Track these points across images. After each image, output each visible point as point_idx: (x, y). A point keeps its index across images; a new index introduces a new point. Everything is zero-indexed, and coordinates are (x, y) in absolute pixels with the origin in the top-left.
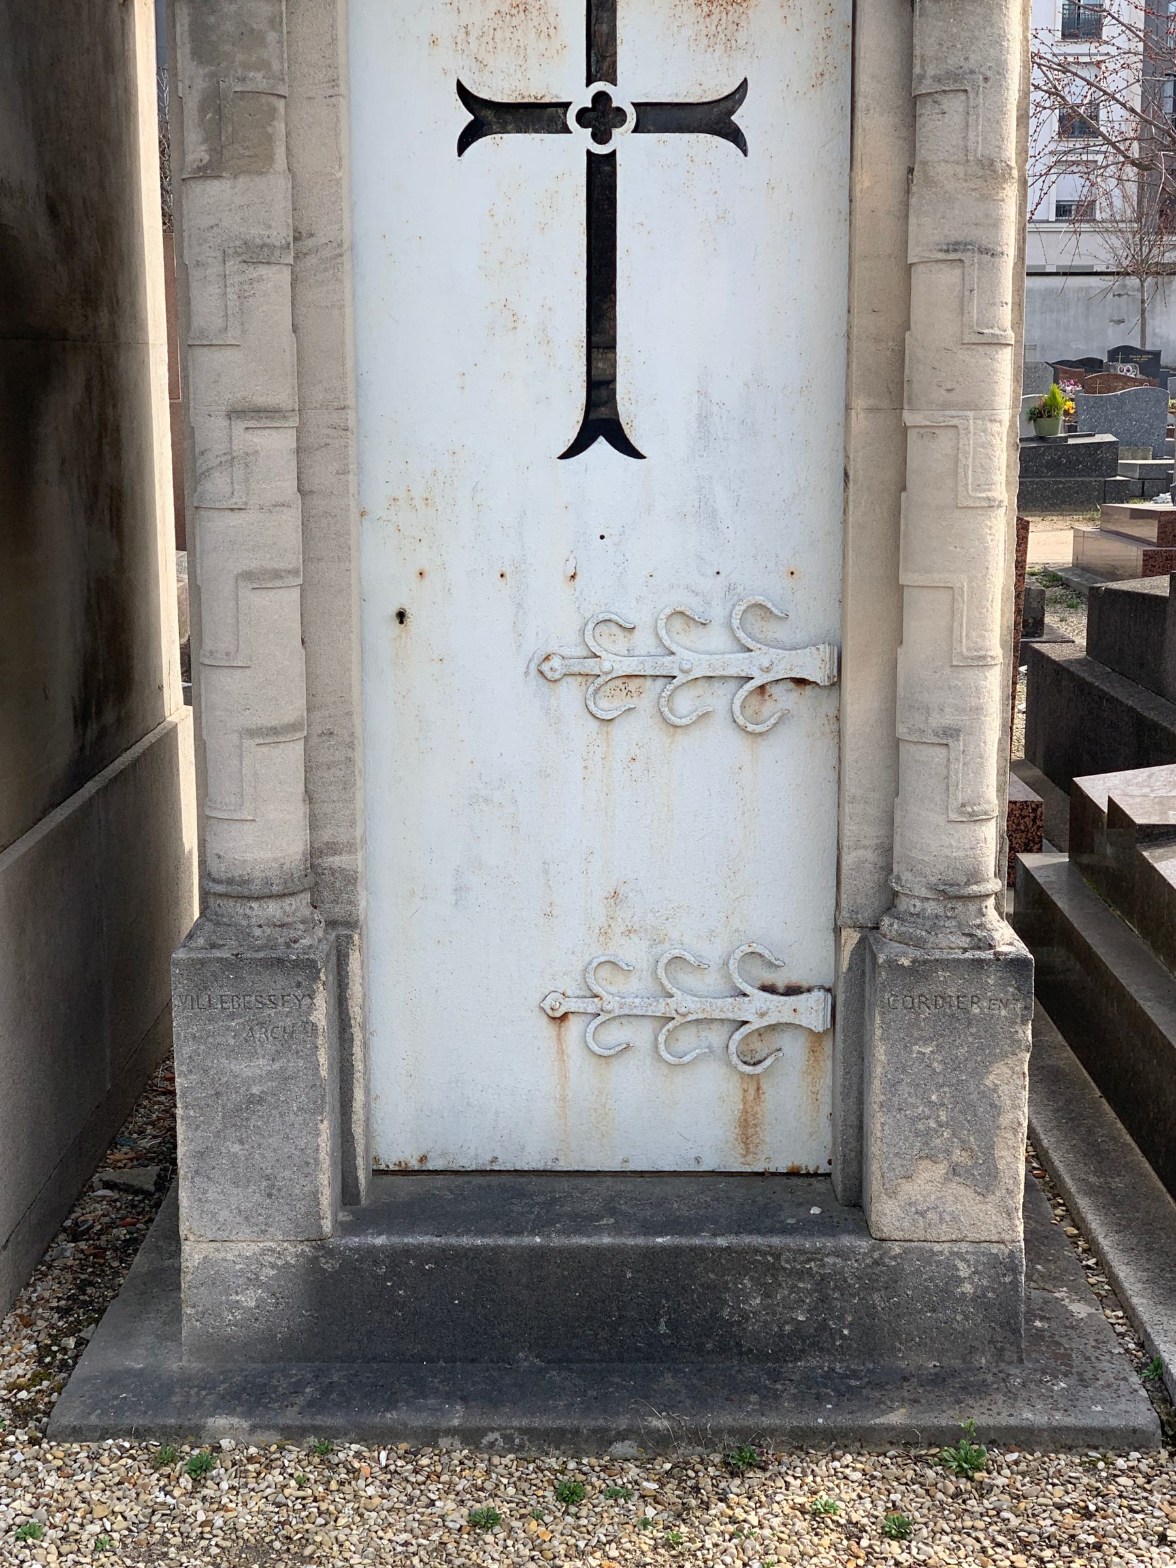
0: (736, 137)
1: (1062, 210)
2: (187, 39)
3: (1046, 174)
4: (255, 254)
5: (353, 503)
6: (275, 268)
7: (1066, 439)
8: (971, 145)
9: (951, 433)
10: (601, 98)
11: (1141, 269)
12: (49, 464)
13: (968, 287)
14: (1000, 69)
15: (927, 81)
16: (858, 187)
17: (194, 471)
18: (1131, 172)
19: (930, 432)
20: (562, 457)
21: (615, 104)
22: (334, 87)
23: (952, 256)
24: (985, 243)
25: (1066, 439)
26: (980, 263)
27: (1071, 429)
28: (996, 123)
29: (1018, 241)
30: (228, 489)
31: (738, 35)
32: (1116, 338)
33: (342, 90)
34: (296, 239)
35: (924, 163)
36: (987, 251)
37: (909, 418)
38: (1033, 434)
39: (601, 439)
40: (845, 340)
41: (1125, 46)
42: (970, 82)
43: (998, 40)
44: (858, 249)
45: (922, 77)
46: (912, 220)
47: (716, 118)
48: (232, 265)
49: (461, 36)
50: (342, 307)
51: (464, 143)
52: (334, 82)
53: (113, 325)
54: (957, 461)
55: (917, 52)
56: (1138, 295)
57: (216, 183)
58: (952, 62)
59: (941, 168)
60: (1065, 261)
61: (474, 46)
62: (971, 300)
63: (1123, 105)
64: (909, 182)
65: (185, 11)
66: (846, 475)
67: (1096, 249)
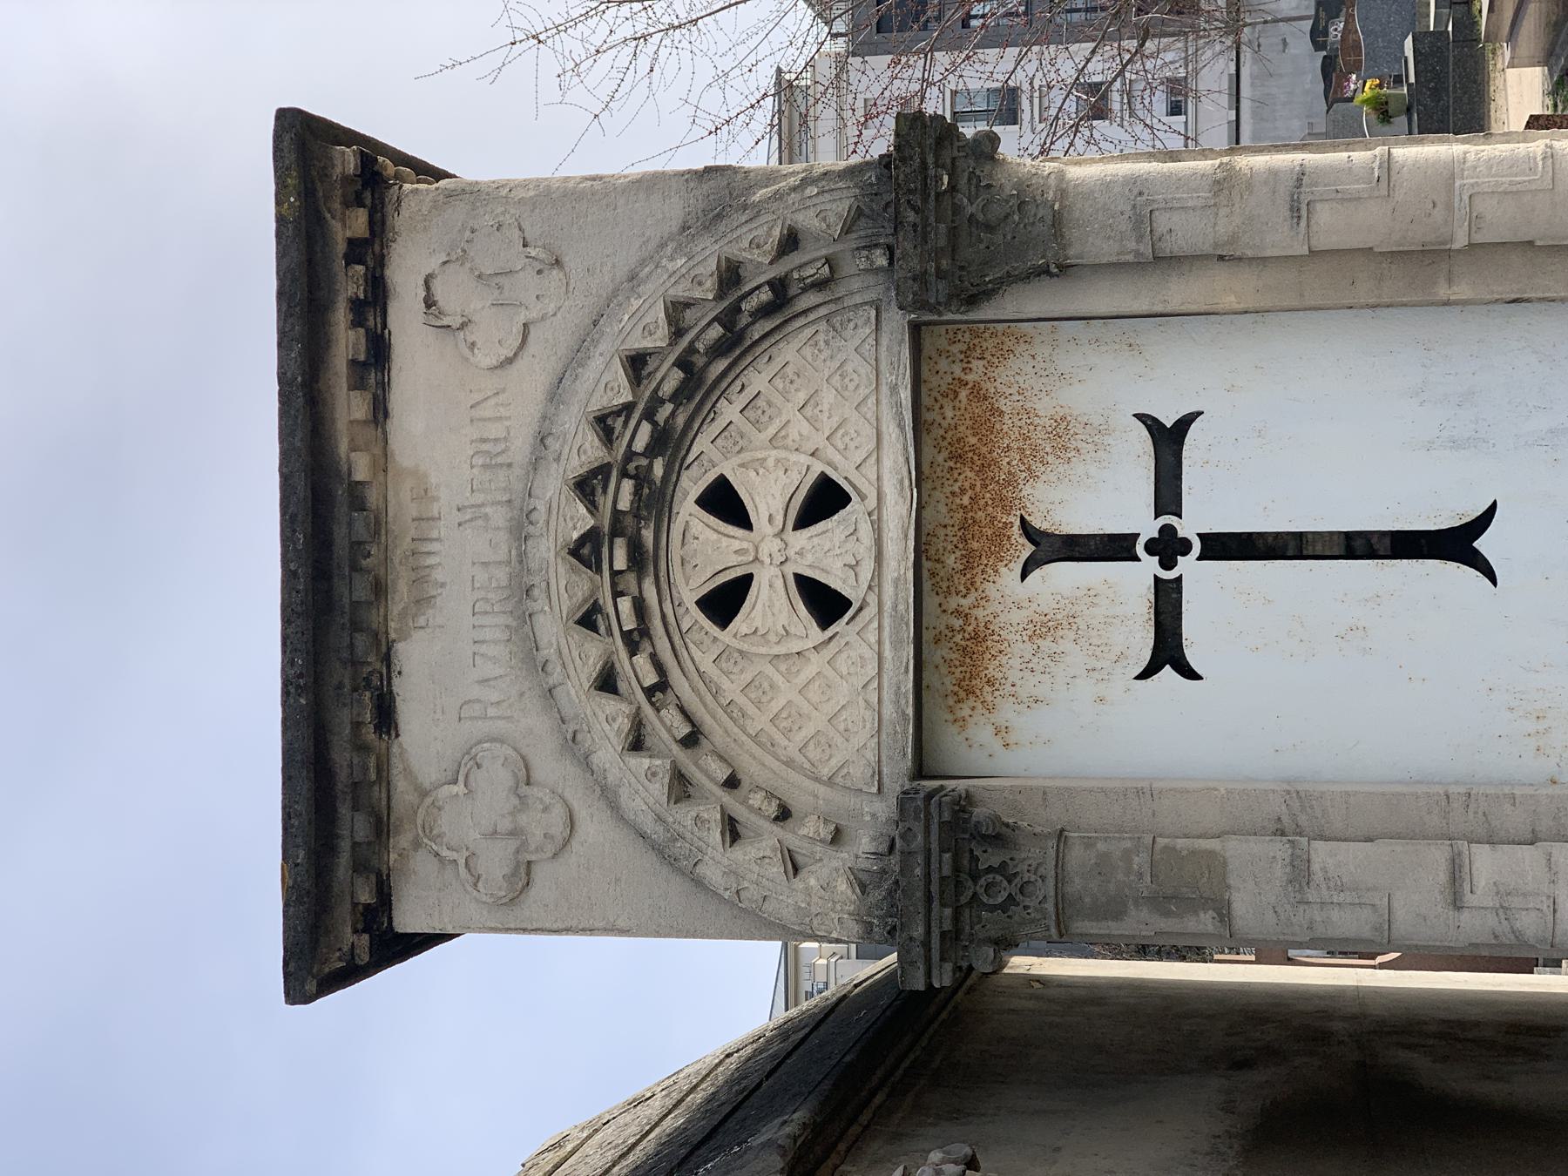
0: (1185, 423)
1: (1175, 109)
2: (1104, 924)
3: (1151, 128)
4: (1300, 873)
5: (1544, 791)
6: (1313, 856)
7: (1409, 85)
8: (1201, 202)
9: (1477, 201)
10: (1151, 548)
11: (1233, 27)
12: (1492, 1090)
13: (1334, 195)
14: (1132, 181)
15: (1142, 248)
16: (1236, 307)
17: (1511, 946)
18: (1150, 45)
19: (1475, 221)
20: (1494, 583)
21: (1156, 535)
22: (1144, 792)
23: (1304, 213)
24: (1291, 183)
25: (1409, 85)
26: (1311, 185)
27: (1398, 80)
28: (1180, 181)
29: (1287, 152)
30: (1533, 914)
31: (1096, 424)
32: (1301, 45)
33: (1145, 784)
34: (1283, 834)
35: (1216, 245)
36: (1300, 180)
37: (1460, 242)
38: (1404, 119)
39: (1475, 544)
40: (1378, 310)
41: (1035, 63)
42: (1142, 206)
43: (1107, 185)
44: (1295, 304)
45: (1137, 253)
46: (1268, 253)
47: (1168, 440)
48: (1311, 895)
49: (1096, 675)
50: (1347, 793)
51: (1191, 674)
52: (1139, 792)
53: (1344, 1018)
54: (1506, 193)
55: (1114, 259)
56: (1259, 27)
57: (1234, 905)
58: (1124, 225)
59: (1221, 229)
60: (1224, 100)
61: (1106, 664)
62: (1343, 192)
63: (1088, 60)
64: (1232, 259)
65: (1079, 924)
66: (1514, 301)
67: (1213, 74)
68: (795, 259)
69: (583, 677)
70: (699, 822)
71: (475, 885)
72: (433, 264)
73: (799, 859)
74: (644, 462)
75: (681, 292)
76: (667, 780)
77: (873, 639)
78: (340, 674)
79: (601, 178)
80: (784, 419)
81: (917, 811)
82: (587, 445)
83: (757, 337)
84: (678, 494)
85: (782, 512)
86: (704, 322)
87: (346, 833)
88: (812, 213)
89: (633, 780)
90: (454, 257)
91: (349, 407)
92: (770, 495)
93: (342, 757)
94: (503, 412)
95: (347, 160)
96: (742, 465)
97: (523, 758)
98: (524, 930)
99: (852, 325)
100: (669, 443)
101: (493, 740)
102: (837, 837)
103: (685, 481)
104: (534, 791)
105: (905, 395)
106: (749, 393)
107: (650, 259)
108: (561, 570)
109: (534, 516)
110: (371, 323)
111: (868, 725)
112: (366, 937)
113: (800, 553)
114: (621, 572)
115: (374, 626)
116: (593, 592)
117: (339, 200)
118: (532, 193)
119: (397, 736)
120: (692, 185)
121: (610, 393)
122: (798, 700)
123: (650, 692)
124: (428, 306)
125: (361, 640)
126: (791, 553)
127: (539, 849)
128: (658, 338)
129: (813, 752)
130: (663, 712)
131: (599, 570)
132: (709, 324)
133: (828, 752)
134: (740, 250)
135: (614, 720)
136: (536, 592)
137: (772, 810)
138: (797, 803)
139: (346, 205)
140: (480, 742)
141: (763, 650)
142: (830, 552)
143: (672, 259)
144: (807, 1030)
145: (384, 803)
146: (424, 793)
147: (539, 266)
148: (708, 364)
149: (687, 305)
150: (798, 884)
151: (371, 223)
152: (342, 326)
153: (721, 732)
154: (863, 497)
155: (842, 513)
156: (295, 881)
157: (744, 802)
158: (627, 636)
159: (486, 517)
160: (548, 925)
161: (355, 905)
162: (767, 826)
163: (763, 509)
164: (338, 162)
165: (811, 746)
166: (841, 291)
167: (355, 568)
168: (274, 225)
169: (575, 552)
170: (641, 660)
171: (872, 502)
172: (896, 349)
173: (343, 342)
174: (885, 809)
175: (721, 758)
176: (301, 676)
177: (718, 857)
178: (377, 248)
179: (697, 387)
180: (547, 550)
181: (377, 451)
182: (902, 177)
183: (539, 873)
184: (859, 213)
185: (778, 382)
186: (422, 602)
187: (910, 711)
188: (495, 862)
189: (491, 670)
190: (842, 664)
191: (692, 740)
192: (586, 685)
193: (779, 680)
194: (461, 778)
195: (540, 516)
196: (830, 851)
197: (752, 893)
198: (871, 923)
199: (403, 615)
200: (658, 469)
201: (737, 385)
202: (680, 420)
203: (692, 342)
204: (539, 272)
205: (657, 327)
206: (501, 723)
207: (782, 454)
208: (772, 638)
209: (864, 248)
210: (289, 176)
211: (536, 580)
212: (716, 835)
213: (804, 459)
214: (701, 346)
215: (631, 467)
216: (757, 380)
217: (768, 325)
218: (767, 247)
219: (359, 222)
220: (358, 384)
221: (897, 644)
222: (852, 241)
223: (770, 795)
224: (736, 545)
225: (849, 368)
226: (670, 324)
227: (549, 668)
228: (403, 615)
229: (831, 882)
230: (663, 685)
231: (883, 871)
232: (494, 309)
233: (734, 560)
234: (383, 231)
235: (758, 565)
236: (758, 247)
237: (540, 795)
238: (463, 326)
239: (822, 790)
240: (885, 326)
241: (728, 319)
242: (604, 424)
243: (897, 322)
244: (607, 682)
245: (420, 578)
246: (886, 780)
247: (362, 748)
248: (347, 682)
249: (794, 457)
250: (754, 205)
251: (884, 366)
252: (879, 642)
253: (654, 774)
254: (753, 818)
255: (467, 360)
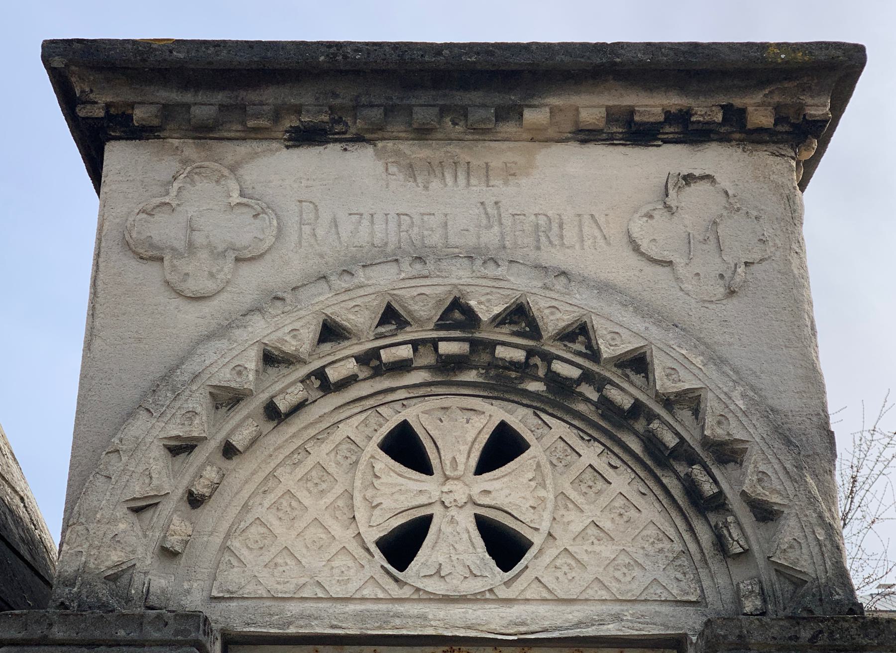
68: (747, 518)
69: (336, 309)
70: (192, 416)
71: (144, 211)
72: (724, 182)
73: (148, 514)
74: (541, 373)
75: (711, 405)
76: (233, 385)
77: (367, 592)
78: (346, 94)
79: (814, 335)
80: (585, 507)
81: (186, 632)
82: (559, 315)
83: (665, 481)
84: (511, 406)
85: (493, 503)
86: (679, 429)
87: (200, 97)
88: (797, 534)
89: (235, 353)
90: (731, 200)
91: (591, 107)
92: (510, 492)
93: (271, 96)
94: (588, 243)
95: (818, 108)
96: (538, 465)
97: (261, 256)
98: (98, 255)
99: (680, 576)
100: (561, 393)
101: (280, 229)
102: (168, 554)
103: (522, 411)
104: (229, 264)
105: (611, 629)
106: (609, 474)
107: (739, 377)
108: (440, 290)
109: (491, 265)
110: (668, 129)
111: (279, 587)
112: (102, 114)
113: (452, 520)
114: (436, 349)
115: (389, 128)
116: (418, 321)
117: (786, 99)
118: (796, 271)
119: (288, 147)
120: (815, 419)
121: (609, 337)
122: (308, 518)
123: (320, 374)
124: (685, 178)
125: (376, 114)
126: (453, 512)
127: (174, 268)
128: (664, 383)
129: (255, 531)
130: (300, 386)
131: (438, 327)
132: (677, 434)
133: (255, 546)
134: (756, 462)
135: (294, 337)
136: (418, 266)
137: (200, 488)
138: (207, 514)
139: (777, 108)
140: (278, 218)
141: (358, 483)
142: (453, 549)
143: (743, 396)
144: (28, 557)
145: (226, 134)
146: (233, 169)
147: (727, 276)
148: (636, 434)
149: (696, 412)
150: (122, 511)
151: (761, 130)
152: (665, 102)
153: (279, 442)
154: (508, 584)
155: (492, 563)
156: (155, 50)
157: (209, 462)
158: (374, 353)
159: (489, 227)
160: (101, 276)
161: (132, 106)
162: (185, 483)
163: (497, 485)
164: (816, 101)
165: (262, 530)
166: (715, 565)
167: (444, 111)
168: (758, 41)
169: (457, 305)
170: (351, 366)
171: (503, 593)
172: (657, 620)
173: (650, 102)
174: (194, 601)
175: (254, 441)
176: (345, 57)
177: (155, 432)
178: (737, 136)
179: (614, 423)
180: (458, 277)
181: (551, 133)
182: (846, 625)
183: (152, 270)
184: (798, 583)
185: (620, 502)
186: (411, 170)
187: (292, 630)
188: (165, 230)
189: (346, 229)
190: (342, 561)
191: (272, 413)
192: (328, 311)
193: (329, 499)
194: (244, 200)
195: (491, 270)
196: (154, 546)
197: (115, 465)
198: (73, 585)
199: (397, 153)
200: (535, 386)
201: (615, 462)
202: (582, 407)
203: (658, 417)
204: (722, 276)
205: (674, 381)
206: (294, 237)
207: (550, 506)
208: (369, 493)
209: (762, 589)
210: (804, 54)
211: (431, 266)
212: (175, 430)
213: (545, 526)
214: (655, 425)
215: (537, 360)
216: (622, 481)
217: (677, 491)
218: (759, 489)
219: (761, 118)
220: (612, 116)
221: (360, 617)
222: (768, 576)
223: (215, 487)
224: (461, 459)
225: (637, 572)
226: (678, 394)
227: (347, 277)
228: (397, 153)
229: (124, 545)
230: (327, 387)
231: (128, 600)
232: (685, 235)
233: (447, 457)
234: (753, 142)
235: (442, 480)
236: (759, 480)
237: (226, 270)
238: (668, 207)
239: (218, 540)
240: (681, 609)
241: (683, 453)
242: (580, 332)
243: (688, 623)
244: (331, 332)
245: (431, 168)
246: (223, 605)
247: (277, 116)
248: (338, 101)
249: (547, 516)
250: (802, 477)
251: (641, 608)
252: (363, 599)
253: (240, 373)
254: (192, 470)
255: (636, 212)
